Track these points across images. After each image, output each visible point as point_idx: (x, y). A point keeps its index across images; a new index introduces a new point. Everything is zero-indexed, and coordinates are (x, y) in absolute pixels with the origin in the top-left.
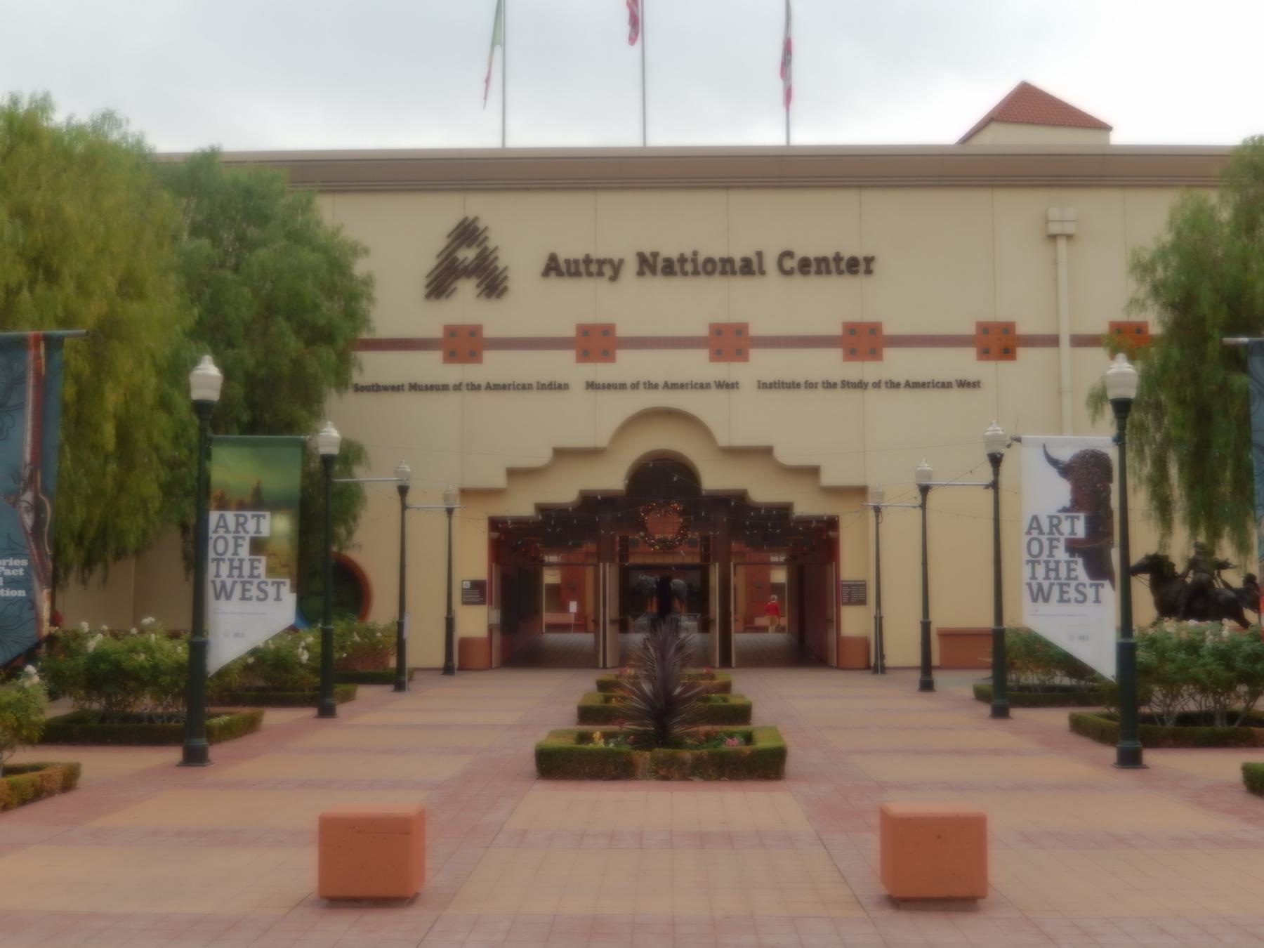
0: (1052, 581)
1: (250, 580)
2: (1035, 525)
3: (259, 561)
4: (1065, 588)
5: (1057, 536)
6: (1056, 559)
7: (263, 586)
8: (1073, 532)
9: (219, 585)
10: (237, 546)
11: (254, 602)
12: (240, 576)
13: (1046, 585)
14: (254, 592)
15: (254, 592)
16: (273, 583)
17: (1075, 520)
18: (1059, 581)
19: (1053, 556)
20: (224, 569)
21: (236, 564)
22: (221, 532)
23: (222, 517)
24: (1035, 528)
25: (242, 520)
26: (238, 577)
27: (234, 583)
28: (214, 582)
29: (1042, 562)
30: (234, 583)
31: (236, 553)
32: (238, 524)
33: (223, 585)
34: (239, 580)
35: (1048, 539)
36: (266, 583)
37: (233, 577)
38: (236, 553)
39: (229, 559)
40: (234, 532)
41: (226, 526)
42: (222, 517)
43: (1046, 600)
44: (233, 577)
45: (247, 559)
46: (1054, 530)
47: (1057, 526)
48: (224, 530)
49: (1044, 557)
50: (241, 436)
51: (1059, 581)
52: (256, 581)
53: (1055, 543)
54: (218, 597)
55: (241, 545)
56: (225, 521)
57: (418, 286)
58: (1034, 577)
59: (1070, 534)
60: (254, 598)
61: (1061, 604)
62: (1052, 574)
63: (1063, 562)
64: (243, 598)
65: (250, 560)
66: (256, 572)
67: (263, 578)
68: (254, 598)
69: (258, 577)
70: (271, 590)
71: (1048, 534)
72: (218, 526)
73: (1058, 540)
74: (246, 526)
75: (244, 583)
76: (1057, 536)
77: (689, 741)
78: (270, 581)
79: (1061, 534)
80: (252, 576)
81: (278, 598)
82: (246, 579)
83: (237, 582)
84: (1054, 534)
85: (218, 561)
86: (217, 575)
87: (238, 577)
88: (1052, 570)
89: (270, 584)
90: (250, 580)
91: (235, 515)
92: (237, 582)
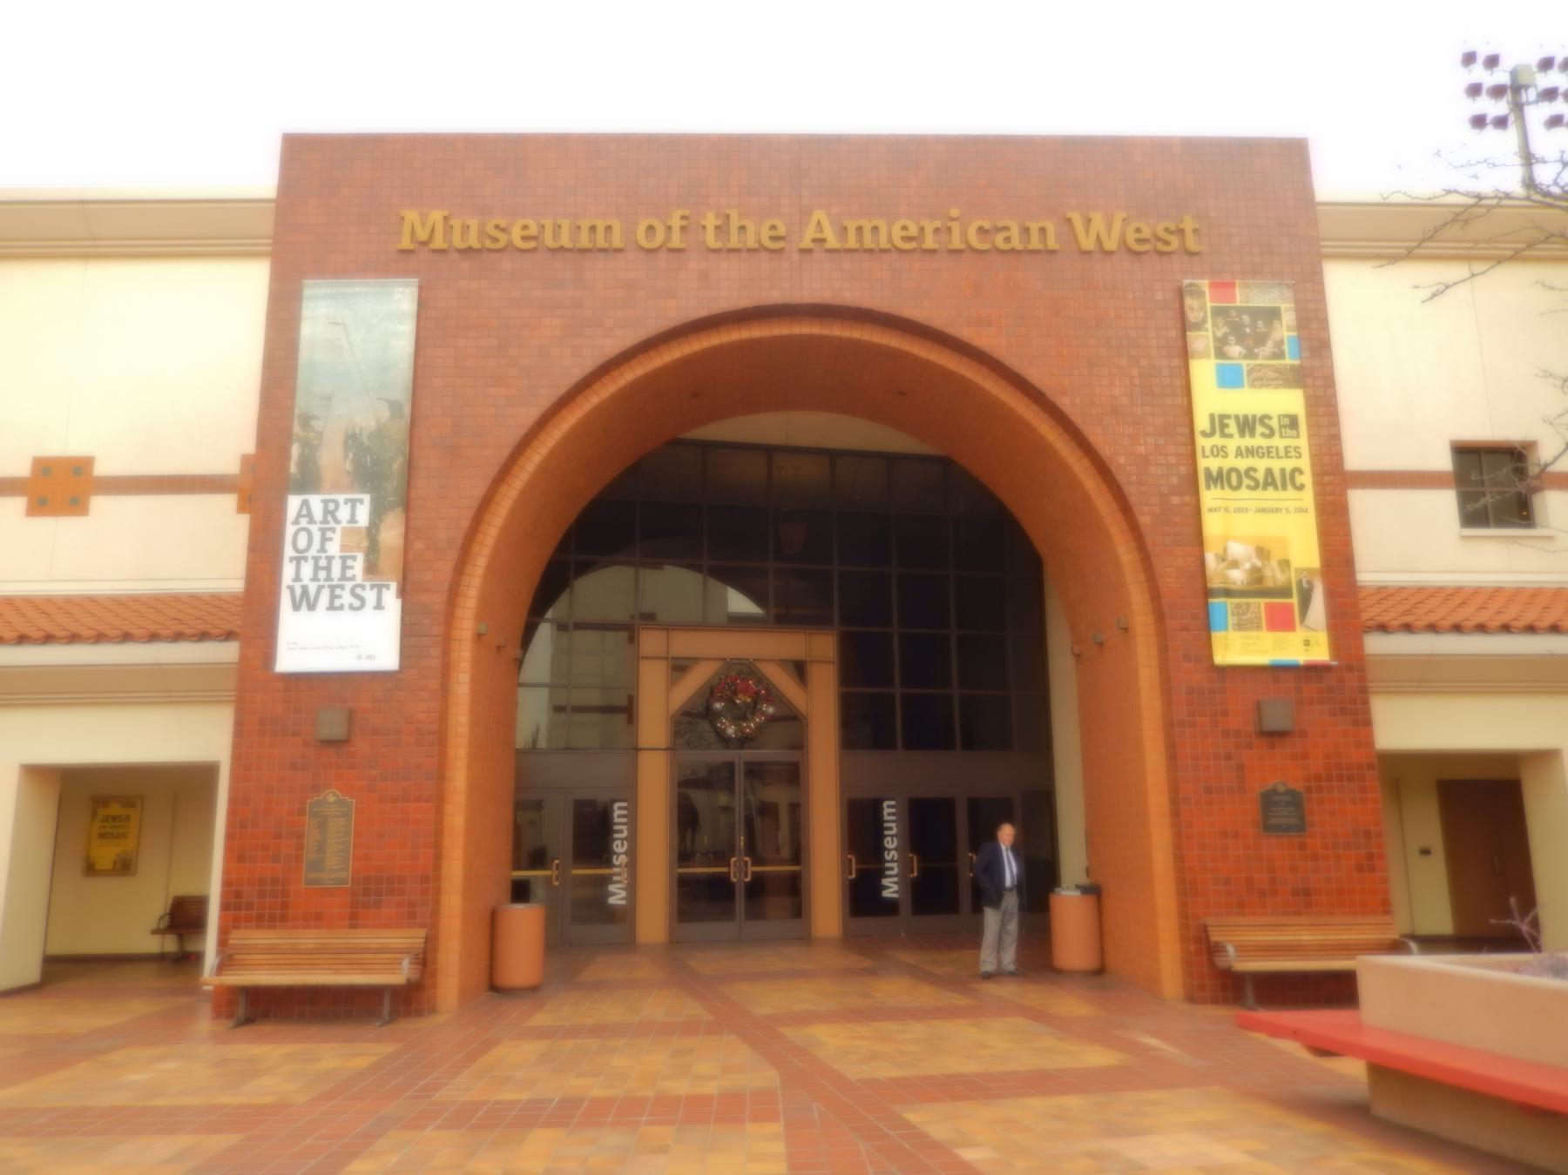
0: (322, 583)
1: (342, 583)
2: (304, 512)
3: (354, 558)
4: (338, 592)
5: (332, 524)
6: (329, 554)
7: (359, 591)
8: (353, 519)
9: (298, 592)
10: (324, 539)
11: (347, 613)
12: (329, 578)
13: (313, 587)
14: (346, 598)
15: (346, 598)
16: (372, 587)
17: (358, 504)
18: (330, 583)
19: (325, 551)
20: (307, 570)
21: (323, 563)
22: (304, 522)
23: (305, 503)
24: (303, 516)
25: (331, 506)
26: (325, 580)
27: (320, 588)
28: (291, 589)
29: (310, 558)
30: (320, 588)
31: (322, 549)
32: (326, 512)
33: (305, 590)
34: (326, 584)
35: (320, 529)
36: (363, 587)
37: (318, 580)
38: (322, 549)
39: (313, 558)
40: (321, 523)
41: (310, 516)
42: (305, 503)
43: (312, 607)
44: (318, 580)
45: (337, 557)
46: (330, 518)
47: (333, 513)
48: (307, 519)
49: (313, 552)
50: (1245, 374)
51: (330, 583)
52: (349, 585)
53: (329, 534)
54: (296, 607)
55: (331, 539)
56: (309, 509)
57: (821, 220)
58: (297, 578)
59: (349, 522)
60: (346, 606)
61: (331, 612)
62: (322, 574)
63: (337, 557)
64: (331, 607)
65: (341, 557)
66: (349, 573)
67: (359, 580)
68: (346, 606)
69: (353, 578)
70: (370, 596)
71: (321, 523)
72: (299, 515)
73: (333, 530)
74: (337, 514)
75: (332, 588)
76: (332, 524)
77: (1283, 804)
78: (368, 584)
79: (337, 521)
80: (343, 577)
81: (379, 606)
82: (336, 582)
83: (323, 587)
84: (328, 523)
85: (298, 560)
86: (297, 578)
87: (325, 580)
88: (323, 568)
89: (368, 587)
90: (342, 583)
91: (323, 501)
92: (323, 587)
